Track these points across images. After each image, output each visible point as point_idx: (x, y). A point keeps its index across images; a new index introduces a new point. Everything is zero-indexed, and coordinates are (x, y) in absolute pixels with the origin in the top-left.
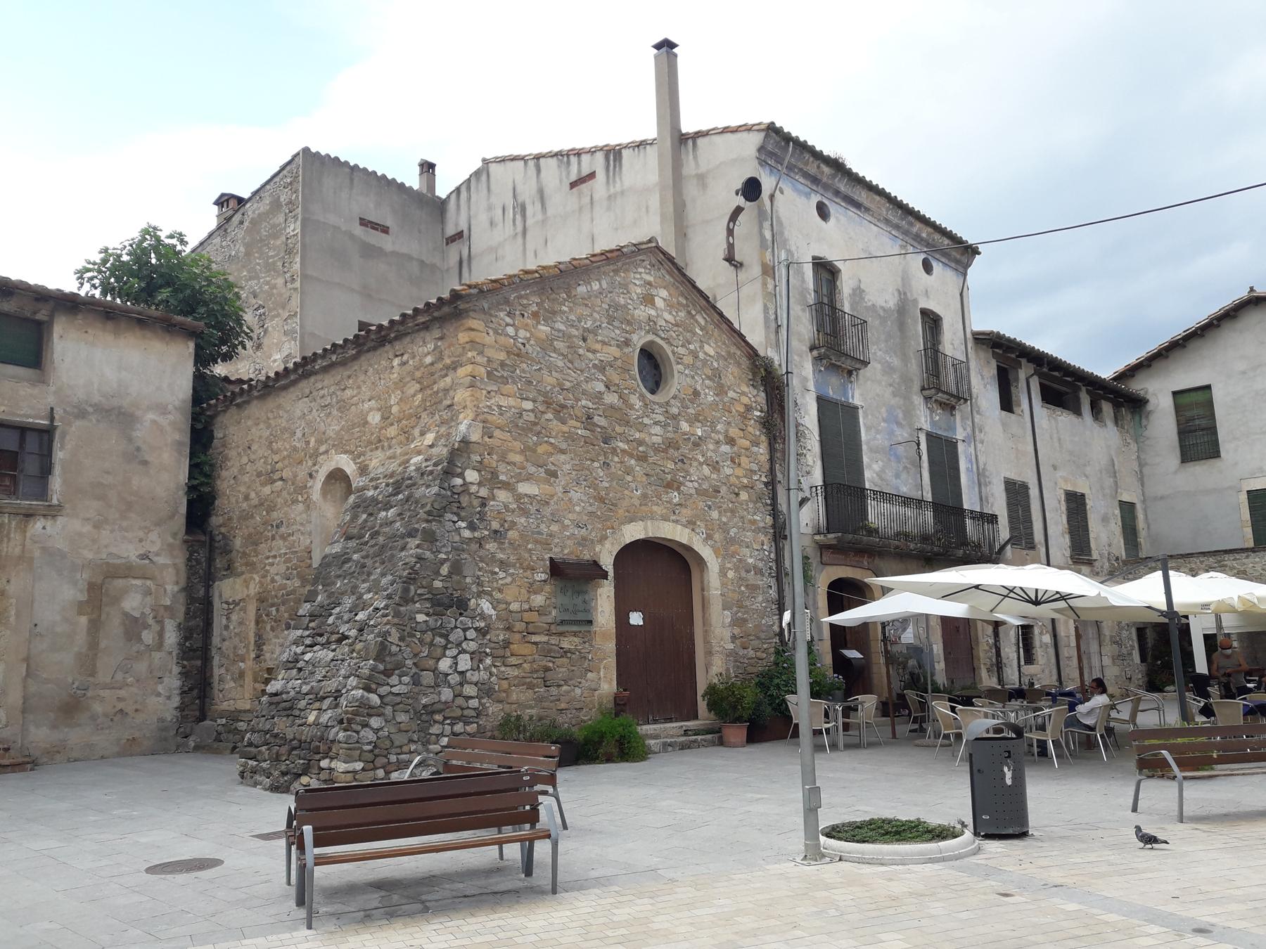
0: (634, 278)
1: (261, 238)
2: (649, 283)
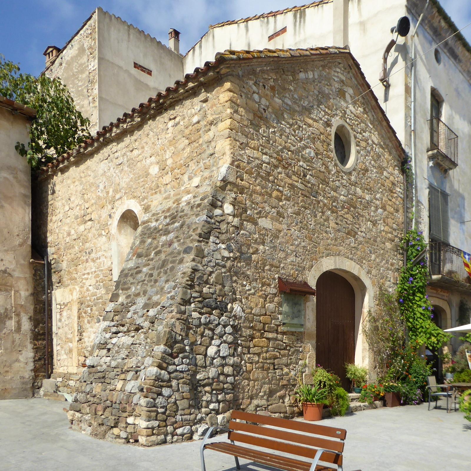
0: (334, 76)
1: (73, 74)
2: (342, 81)
